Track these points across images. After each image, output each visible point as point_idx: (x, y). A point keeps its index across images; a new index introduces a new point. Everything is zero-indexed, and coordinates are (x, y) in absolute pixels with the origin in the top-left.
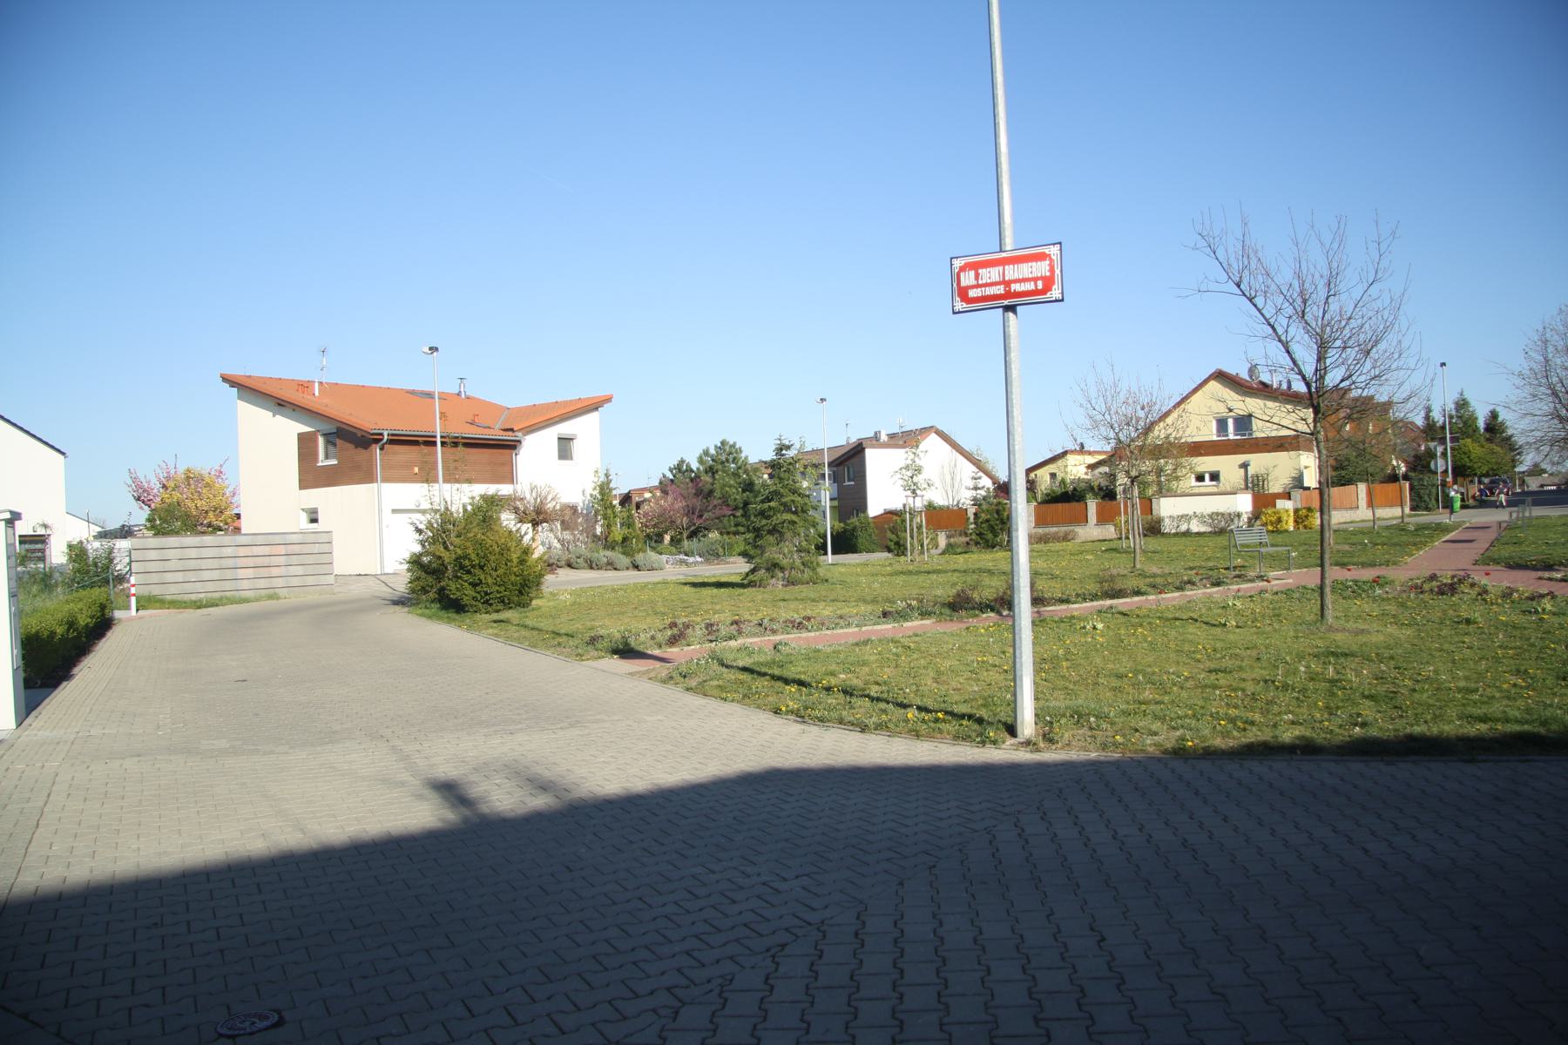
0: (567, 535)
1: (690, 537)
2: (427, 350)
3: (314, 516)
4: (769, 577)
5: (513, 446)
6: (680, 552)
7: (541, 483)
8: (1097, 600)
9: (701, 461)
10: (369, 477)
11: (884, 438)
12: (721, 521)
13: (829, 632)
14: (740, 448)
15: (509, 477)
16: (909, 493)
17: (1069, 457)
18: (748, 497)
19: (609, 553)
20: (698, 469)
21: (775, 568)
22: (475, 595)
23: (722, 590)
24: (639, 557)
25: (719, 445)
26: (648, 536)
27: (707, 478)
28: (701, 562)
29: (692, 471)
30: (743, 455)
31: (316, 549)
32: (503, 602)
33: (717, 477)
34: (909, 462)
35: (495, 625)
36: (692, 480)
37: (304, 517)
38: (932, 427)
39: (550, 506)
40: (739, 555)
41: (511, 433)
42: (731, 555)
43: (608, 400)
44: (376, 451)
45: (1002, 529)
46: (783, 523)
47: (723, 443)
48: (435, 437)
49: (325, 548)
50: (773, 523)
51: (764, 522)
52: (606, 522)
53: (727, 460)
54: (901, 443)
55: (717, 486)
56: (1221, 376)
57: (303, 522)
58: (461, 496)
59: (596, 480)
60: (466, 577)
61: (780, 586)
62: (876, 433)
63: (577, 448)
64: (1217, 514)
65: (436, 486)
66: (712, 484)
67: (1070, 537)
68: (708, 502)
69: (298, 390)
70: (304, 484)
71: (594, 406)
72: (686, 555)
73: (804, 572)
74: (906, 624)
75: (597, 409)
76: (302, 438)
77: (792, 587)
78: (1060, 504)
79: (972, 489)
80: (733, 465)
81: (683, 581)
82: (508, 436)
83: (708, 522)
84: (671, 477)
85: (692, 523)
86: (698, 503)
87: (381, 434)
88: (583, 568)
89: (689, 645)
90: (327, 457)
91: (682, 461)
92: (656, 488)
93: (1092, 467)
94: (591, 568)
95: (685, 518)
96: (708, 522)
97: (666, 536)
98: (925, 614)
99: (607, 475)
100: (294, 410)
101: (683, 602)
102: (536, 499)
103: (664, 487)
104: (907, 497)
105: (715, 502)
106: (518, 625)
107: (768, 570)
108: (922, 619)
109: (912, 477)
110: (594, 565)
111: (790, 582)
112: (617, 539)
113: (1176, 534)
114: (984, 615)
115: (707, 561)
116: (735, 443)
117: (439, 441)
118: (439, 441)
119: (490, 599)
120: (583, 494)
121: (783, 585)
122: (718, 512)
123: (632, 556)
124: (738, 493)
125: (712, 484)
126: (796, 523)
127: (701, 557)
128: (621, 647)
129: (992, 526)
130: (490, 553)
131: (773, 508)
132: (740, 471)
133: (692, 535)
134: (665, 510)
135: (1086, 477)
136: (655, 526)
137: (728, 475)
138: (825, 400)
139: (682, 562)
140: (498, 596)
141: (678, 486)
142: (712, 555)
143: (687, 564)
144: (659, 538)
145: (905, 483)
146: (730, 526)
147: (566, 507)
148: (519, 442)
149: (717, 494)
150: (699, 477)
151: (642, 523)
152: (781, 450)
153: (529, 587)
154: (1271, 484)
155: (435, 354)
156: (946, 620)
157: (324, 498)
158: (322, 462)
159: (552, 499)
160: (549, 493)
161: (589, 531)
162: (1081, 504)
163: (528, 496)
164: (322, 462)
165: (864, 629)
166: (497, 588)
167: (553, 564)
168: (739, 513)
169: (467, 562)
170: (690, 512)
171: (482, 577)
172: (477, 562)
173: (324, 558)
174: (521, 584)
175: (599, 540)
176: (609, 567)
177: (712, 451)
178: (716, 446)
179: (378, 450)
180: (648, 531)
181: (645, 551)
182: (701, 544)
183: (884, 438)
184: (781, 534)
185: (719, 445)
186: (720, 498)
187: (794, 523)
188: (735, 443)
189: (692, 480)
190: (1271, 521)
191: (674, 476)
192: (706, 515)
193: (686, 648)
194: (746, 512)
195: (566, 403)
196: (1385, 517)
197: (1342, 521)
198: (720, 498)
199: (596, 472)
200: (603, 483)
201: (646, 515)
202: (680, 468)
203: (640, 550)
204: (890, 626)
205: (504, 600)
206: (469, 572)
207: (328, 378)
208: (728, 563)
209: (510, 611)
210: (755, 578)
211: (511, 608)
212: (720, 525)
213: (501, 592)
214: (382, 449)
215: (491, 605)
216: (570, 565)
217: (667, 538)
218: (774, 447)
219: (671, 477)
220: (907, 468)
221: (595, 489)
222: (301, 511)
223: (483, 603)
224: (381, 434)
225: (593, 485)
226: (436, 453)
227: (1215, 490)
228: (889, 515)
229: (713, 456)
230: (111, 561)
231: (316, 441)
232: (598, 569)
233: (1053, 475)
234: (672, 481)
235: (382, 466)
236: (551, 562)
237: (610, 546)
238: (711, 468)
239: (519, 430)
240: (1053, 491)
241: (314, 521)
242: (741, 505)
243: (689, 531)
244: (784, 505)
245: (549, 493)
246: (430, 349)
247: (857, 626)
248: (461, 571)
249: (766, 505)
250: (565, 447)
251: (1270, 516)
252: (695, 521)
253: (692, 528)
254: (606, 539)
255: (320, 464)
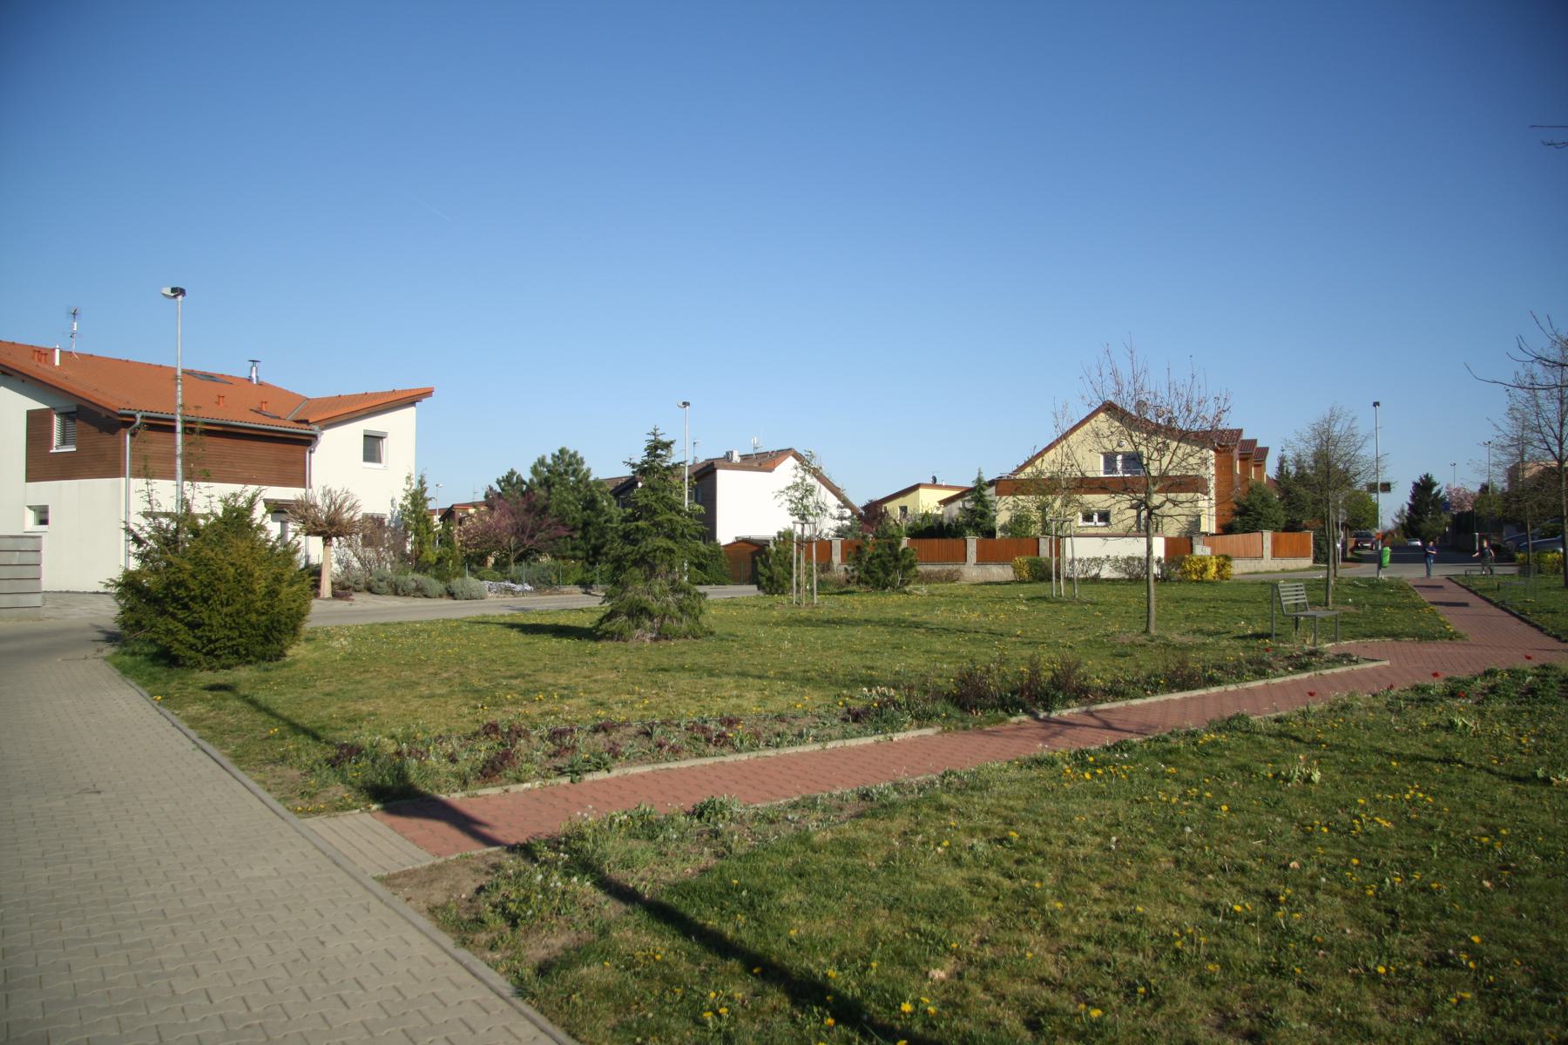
0: (370, 553)
1: (518, 560)
2: (167, 291)
3: (43, 517)
4: (633, 626)
5: (308, 441)
6: (506, 579)
7: (337, 487)
8: (1154, 692)
9: (535, 471)
10: (114, 470)
11: (736, 459)
12: (556, 544)
13: (771, 753)
14: (582, 459)
15: (299, 477)
16: (796, 518)
17: (921, 490)
18: (589, 516)
19: (418, 576)
20: (531, 480)
21: (641, 614)
22: (191, 640)
23: (565, 641)
24: (456, 583)
25: (557, 453)
26: (468, 557)
27: (542, 492)
28: (531, 592)
29: (524, 483)
30: (585, 467)
31: (16, 558)
32: (237, 652)
33: (553, 491)
34: (799, 481)
35: (209, 695)
36: (523, 494)
37: (30, 517)
38: (790, 449)
39: (346, 516)
40: (576, 584)
41: (304, 426)
42: (566, 584)
43: (428, 393)
44: (125, 437)
45: (896, 567)
46: (655, 551)
47: (562, 451)
48: (174, 421)
49: (31, 558)
50: (642, 551)
51: (628, 548)
52: (418, 538)
53: (566, 472)
54: (756, 465)
55: (553, 501)
56: (1109, 408)
57: (29, 522)
58: (209, 498)
59: (408, 487)
60: (181, 614)
61: (648, 641)
62: (727, 453)
63: (387, 447)
64: (1133, 559)
65: (123, 479)
66: (548, 499)
67: (954, 578)
68: (541, 519)
69: (33, 358)
70: (33, 475)
71: (409, 400)
72: (513, 582)
73: (681, 621)
74: (897, 737)
75: (412, 403)
76: (32, 416)
77: (663, 642)
78: (936, 540)
79: (838, 519)
80: (572, 479)
81: (508, 620)
82: (302, 429)
83: (540, 544)
84: (499, 490)
85: (520, 544)
86: (530, 521)
87: (133, 416)
88: (386, 594)
89: (519, 781)
90: (64, 442)
91: (512, 473)
92: (481, 504)
93: (946, 502)
94: (396, 594)
95: (513, 539)
96: (540, 544)
97: (489, 558)
98: (923, 718)
99: (421, 483)
100: (23, 381)
101: (510, 664)
102: (329, 508)
103: (491, 501)
104: (794, 523)
105: (550, 521)
106: (244, 697)
107: (630, 615)
108: (919, 727)
109: (802, 499)
110: (400, 590)
111: (662, 635)
112: (430, 559)
113: (1085, 580)
114: (1014, 719)
115: (538, 590)
116: (576, 453)
117: (179, 427)
118: (179, 427)
119: (216, 649)
120: (392, 504)
121: (651, 639)
122: (553, 532)
123: (447, 581)
124: (577, 511)
125: (548, 499)
126: (673, 552)
127: (530, 585)
128: (389, 781)
129: (884, 564)
130: (218, 579)
131: (643, 529)
132: (581, 485)
133: (521, 558)
134: (490, 527)
135: (935, 512)
136: (477, 546)
137: (566, 489)
138: (689, 404)
139: (508, 590)
140: (229, 644)
141: (506, 500)
142: (544, 583)
143: (513, 593)
144: (481, 560)
145: (793, 506)
146: (567, 549)
147: (370, 518)
148: (315, 436)
149: (553, 511)
150: (532, 490)
151: (461, 541)
152: (656, 448)
153: (280, 632)
154: (1165, 527)
155: (180, 298)
156: (957, 728)
157: (56, 492)
158: (56, 447)
159: (348, 509)
160: (344, 501)
161: (398, 548)
162: (959, 541)
163: (319, 502)
164: (56, 447)
165: (830, 745)
166: (227, 632)
167: (349, 587)
168: (577, 535)
169: (182, 593)
170: (519, 531)
171: (205, 615)
172: (198, 592)
173: (28, 572)
174: (266, 626)
175: (409, 560)
176: (419, 593)
177: (549, 461)
178: (553, 455)
179: (128, 437)
180: (468, 551)
181: (463, 576)
182: (531, 569)
183: (736, 459)
184: (653, 568)
185: (557, 453)
186: (556, 516)
187: (670, 551)
188: (576, 453)
189: (523, 494)
190: (1196, 569)
191: (503, 490)
192: (538, 536)
193: (514, 788)
194: (585, 534)
195: (375, 396)
196: (1290, 568)
197: (1246, 570)
198: (556, 516)
199: (409, 478)
200: (416, 491)
201: (466, 532)
202: (510, 481)
203: (458, 574)
204: (870, 740)
205: (238, 649)
206: (186, 607)
207: (75, 347)
208: (563, 593)
209: (248, 668)
210: (614, 628)
211: (250, 662)
212: (555, 548)
213: (233, 639)
214: (133, 435)
215: (218, 657)
216: (370, 589)
217: (491, 560)
218: (645, 445)
219: (499, 490)
220: (795, 487)
221: (405, 498)
222: (27, 509)
223: (207, 654)
224: (133, 416)
225: (404, 494)
226: (174, 441)
227: (1105, 531)
228: (742, 544)
229: (549, 466)
230: (1328, 464)
231: (51, 421)
232: (405, 595)
233: (904, 509)
234: (499, 494)
235: (132, 457)
236: (347, 584)
237: (421, 567)
238: (546, 480)
239: (314, 423)
240: (916, 524)
241: (44, 522)
242: (581, 526)
243: (517, 554)
244: (658, 525)
245: (344, 501)
246: (173, 290)
247: (816, 739)
248: (174, 605)
249: (633, 525)
250: (372, 447)
251: (1195, 563)
252: (525, 541)
253: (522, 550)
254: (417, 559)
255: (54, 450)
